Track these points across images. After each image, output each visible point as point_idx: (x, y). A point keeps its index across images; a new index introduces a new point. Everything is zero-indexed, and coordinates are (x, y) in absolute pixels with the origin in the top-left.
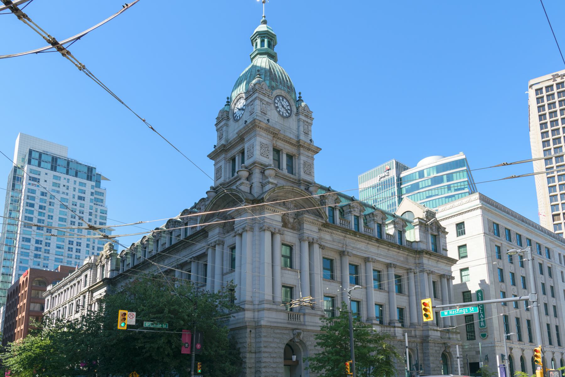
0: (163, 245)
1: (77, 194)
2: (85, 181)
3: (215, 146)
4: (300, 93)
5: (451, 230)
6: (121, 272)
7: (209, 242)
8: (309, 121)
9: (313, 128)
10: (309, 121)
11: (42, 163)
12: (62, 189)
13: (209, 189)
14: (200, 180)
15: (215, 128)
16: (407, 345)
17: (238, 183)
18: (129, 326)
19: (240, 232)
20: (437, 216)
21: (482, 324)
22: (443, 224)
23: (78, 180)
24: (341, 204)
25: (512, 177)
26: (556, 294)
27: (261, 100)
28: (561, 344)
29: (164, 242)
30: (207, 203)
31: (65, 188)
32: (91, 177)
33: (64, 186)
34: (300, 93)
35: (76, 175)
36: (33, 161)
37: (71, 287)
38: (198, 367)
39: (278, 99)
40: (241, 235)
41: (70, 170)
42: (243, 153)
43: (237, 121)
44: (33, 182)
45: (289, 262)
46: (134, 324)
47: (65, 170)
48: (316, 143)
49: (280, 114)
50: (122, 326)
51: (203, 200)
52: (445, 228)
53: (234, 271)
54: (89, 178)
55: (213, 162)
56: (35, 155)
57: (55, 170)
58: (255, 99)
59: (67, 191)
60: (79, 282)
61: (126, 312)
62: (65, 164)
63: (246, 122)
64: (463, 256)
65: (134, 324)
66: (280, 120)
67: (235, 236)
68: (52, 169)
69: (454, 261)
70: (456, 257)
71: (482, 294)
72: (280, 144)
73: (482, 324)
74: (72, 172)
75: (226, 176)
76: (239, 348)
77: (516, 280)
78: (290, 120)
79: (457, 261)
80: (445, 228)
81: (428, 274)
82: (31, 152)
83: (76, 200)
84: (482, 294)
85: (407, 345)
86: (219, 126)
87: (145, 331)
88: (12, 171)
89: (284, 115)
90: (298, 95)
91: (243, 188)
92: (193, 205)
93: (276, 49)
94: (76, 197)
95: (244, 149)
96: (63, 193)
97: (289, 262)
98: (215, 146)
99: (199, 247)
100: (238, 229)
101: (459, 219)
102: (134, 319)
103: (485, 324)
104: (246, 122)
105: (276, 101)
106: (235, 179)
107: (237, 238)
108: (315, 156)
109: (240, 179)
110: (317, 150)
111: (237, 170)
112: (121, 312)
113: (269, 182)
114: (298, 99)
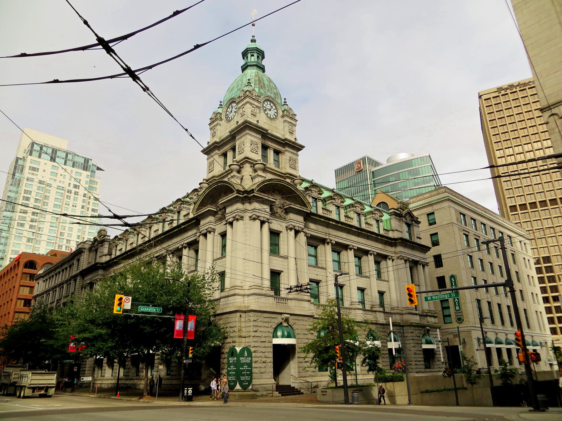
0: (155, 231)
1: (73, 182)
2: (81, 171)
3: (208, 142)
4: (285, 99)
5: (423, 220)
6: (113, 256)
7: (201, 230)
8: (293, 122)
9: (297, 129)
10: (293, 122)
11: (43, 155)
12: (59, 178)
13: (202, 181)
14: (193, 172)
15: (209, 127)
16: (392, 329)
17: (229, 176)
18: (125, 311)
19: (231, 220)
20: (411, 206)
21: (457, 308)
22: (415, 214)
23: (75, 170)
24: (323, 196)
25: (150, 67)
26: (521, 280)
27: (251, 104)
28: (531, 327)
29: (157, 229)
30: (200, 193)
31: (62, 177)
32: (87, 167)
33: (61, 175)
34: (285, 99)
35: (73, 166)
36: (34, 153)
37: (63, 270)
38: (190, 352)
39: (266, 103)
40: (231, 224)
41: (68, 162)
42: (234, 149)
43: (229, 121)
44: (32, 172)
45: (274, 249)
46: (129, 308)
47: (38, 154)
48: (299, 142)
49: (268, 116)
50: (116, 309)
51: (195, 190)
52: (418, 218)
53: (225, 257)
54: (85, 168)
55: (206, 156)
56: (36, 147)
57: (54, 161)
58: (246, 103)
59: (63, 180)
60: (70, 266)
61: (122, 296)
62: (64, 155)
63: (238, 122)
64: (436, 243)
65: (129, 308)
66: (269, 121)
67: (226, 224)
68: (51, 161)
69: (425, 249)
70: (430, 245)
71: (455, 279)
72: (269, 143)
73: (457, 308)
74: (70, 163)
75: (218, 170)
76: (378, 362)
77: (484, 266)
78: (277, 121)
79: (430, 248)
80: (418, 218)
81: (424, 266)
82: (33, 144)
83: (71, 188)
84: (455, 279)
85: (392, 329)
86: (212, 126)
87: (140, 315)
88: (13, 162)
89: (272, 117)
90: (283, 101)
91: (233, 180)
92: (185, 194)
93: (264, 62)
94: (72, 185)
95: (235, 146)
96: (60, 182)
97: (274, 249)
98: (208, 142)
99: (189, 236)
100: (229, 217)
101: (429, 210)
102: (130, 304)
103: (459, 308)
104: (238, 122)
105: (265, 105)
106: (227, 172)
107: (229, 227)
108: (300, 153)
109: (231, 172)
110: (298, 148)
111: (228, 164)
112: (118, 296)
113: (258, 175)
114: (283, 104)
